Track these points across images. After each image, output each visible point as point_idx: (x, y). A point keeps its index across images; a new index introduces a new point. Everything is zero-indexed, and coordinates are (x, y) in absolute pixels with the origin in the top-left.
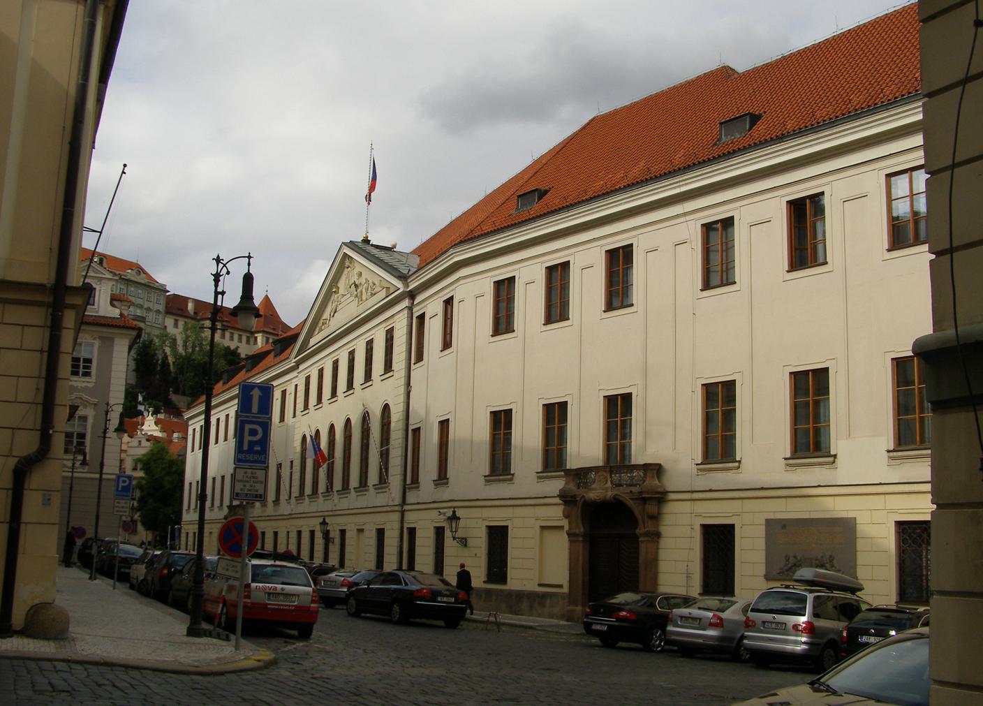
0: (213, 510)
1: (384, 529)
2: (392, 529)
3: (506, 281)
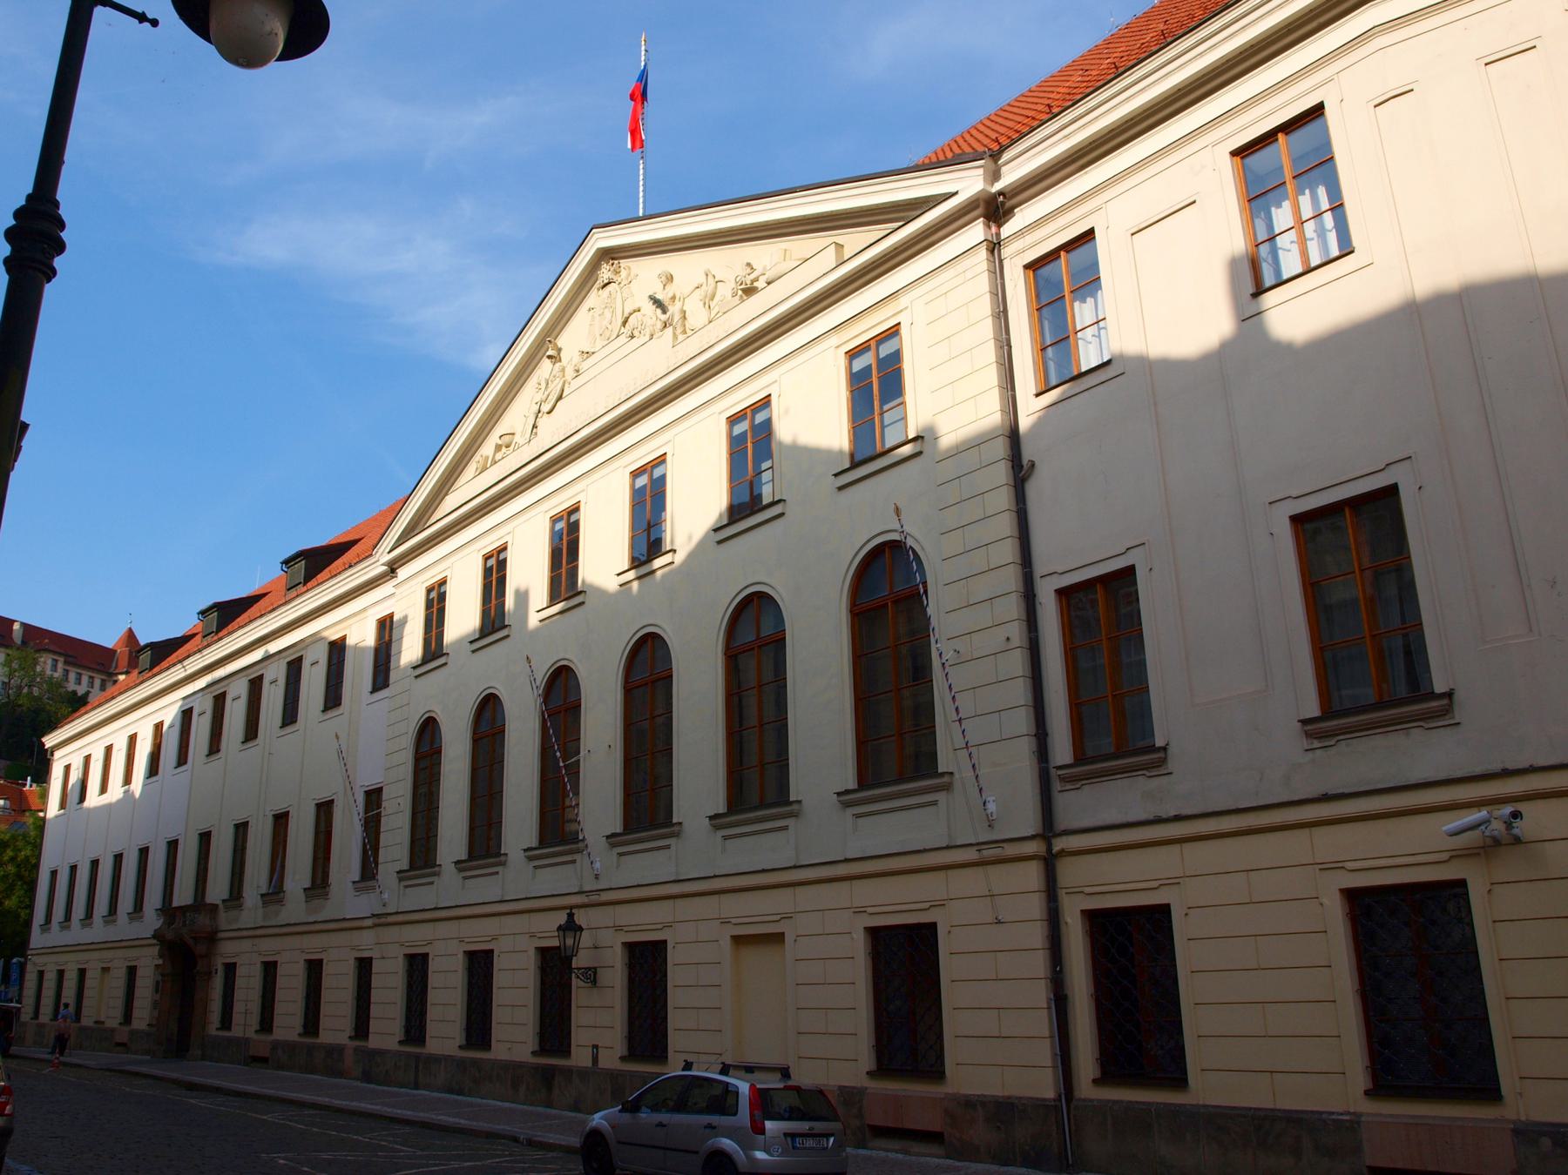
0: (68, 927)
1: (492, 951)
2: (999, 922)
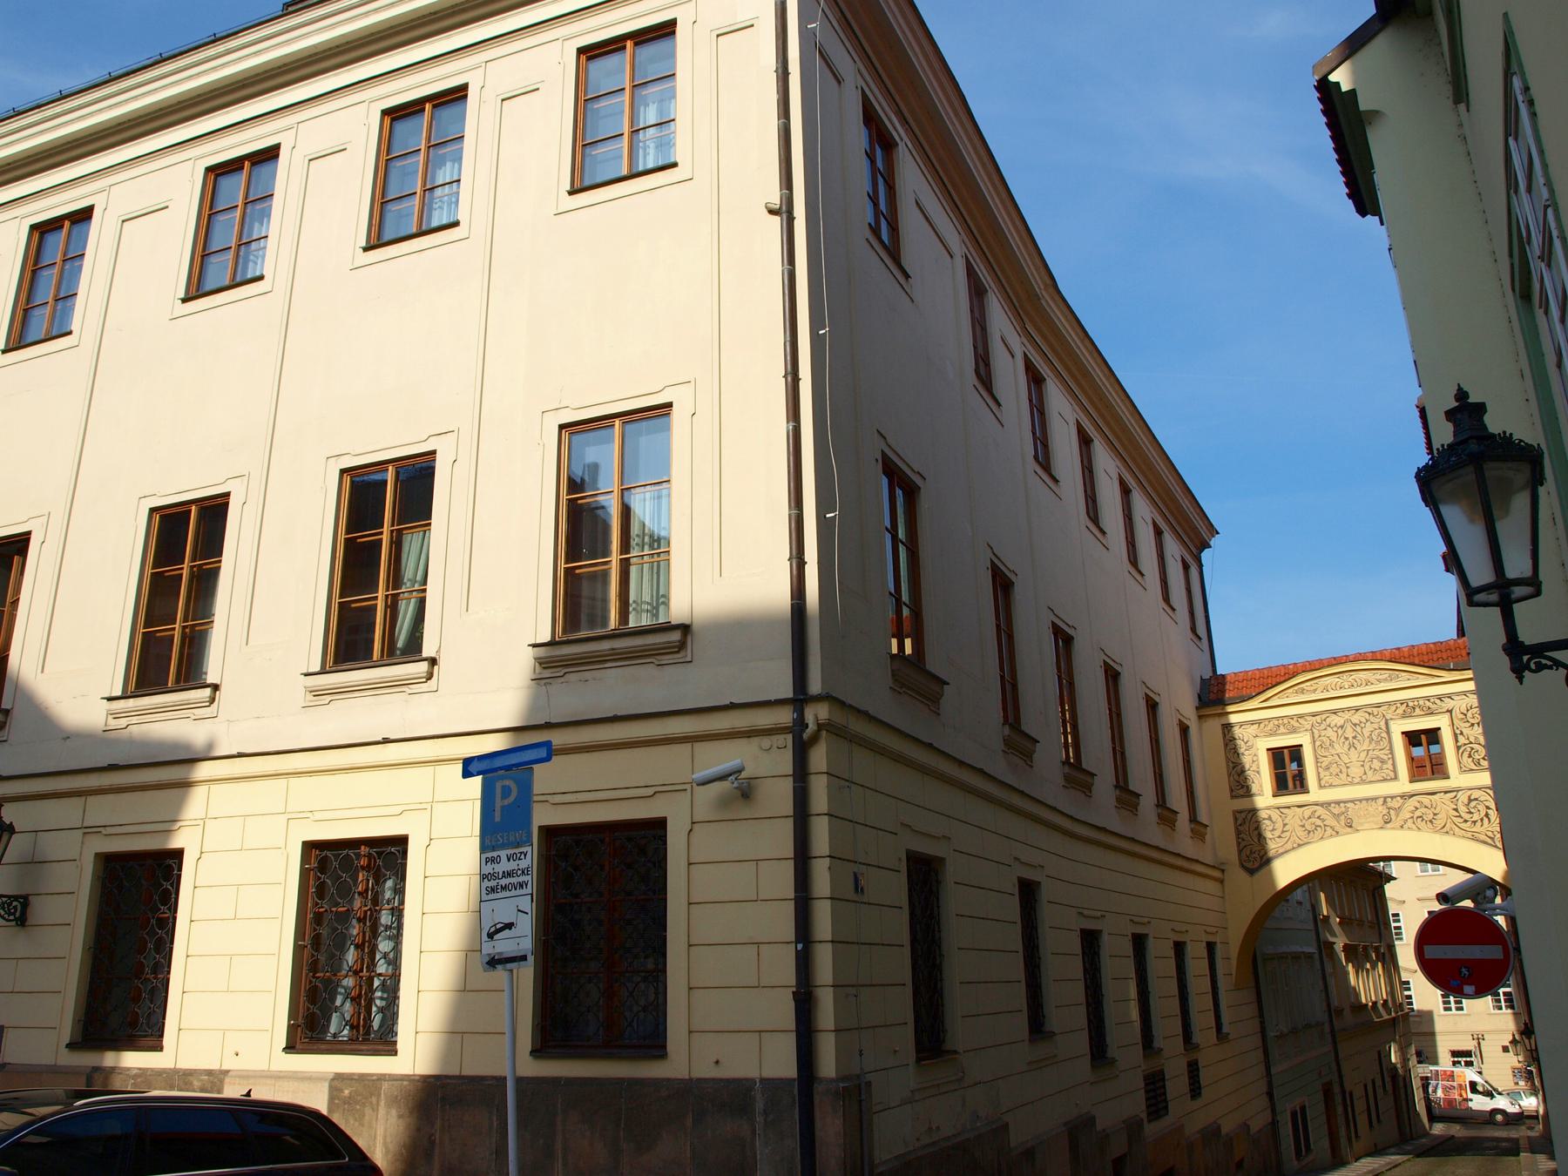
3: (67, 224)
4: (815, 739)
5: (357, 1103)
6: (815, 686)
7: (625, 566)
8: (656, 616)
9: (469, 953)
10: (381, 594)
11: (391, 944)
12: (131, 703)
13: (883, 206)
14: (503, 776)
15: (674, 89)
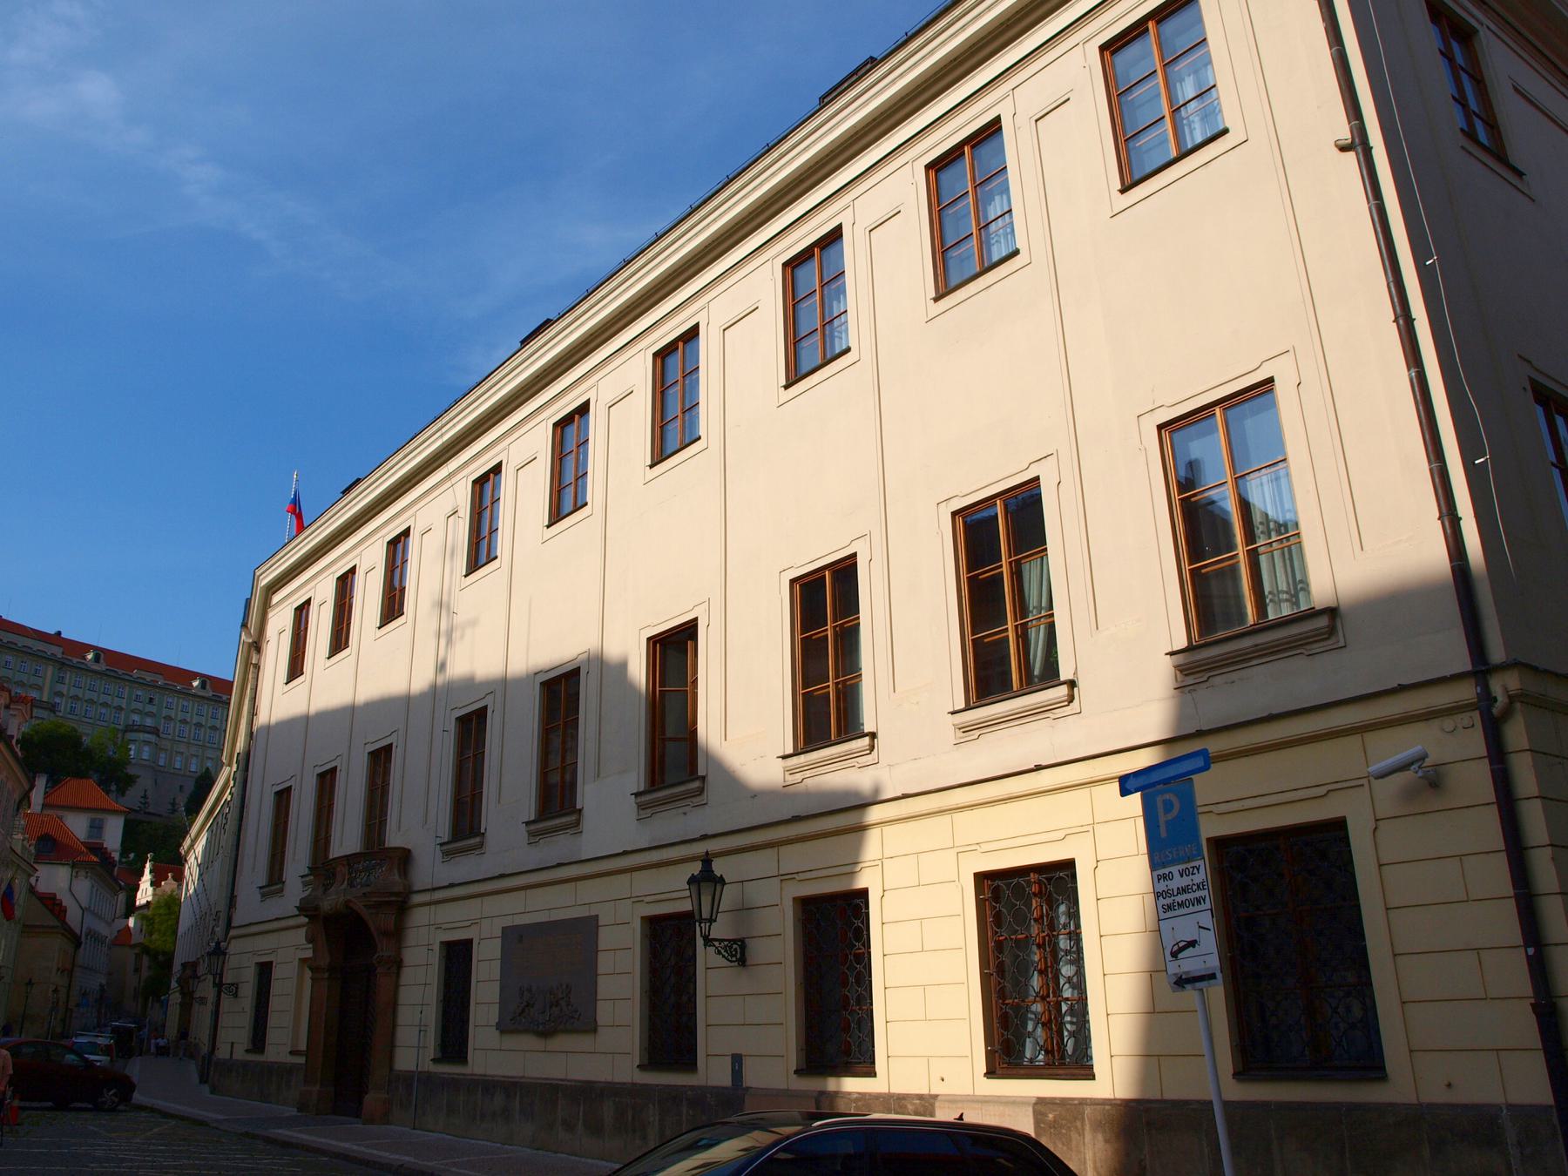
3: (680, 344)
4: (1507, 713)
5: (1062, 1127)
6: (1497, 652)
7: (1253, 556)
8: (1297, 604)
9: (1154, 974)
10: (1010, 625)
11: (1074, 968)
12: (803, 759)
13: (1473, 105)
14: (1163, 790)
15: (1208, 55)
